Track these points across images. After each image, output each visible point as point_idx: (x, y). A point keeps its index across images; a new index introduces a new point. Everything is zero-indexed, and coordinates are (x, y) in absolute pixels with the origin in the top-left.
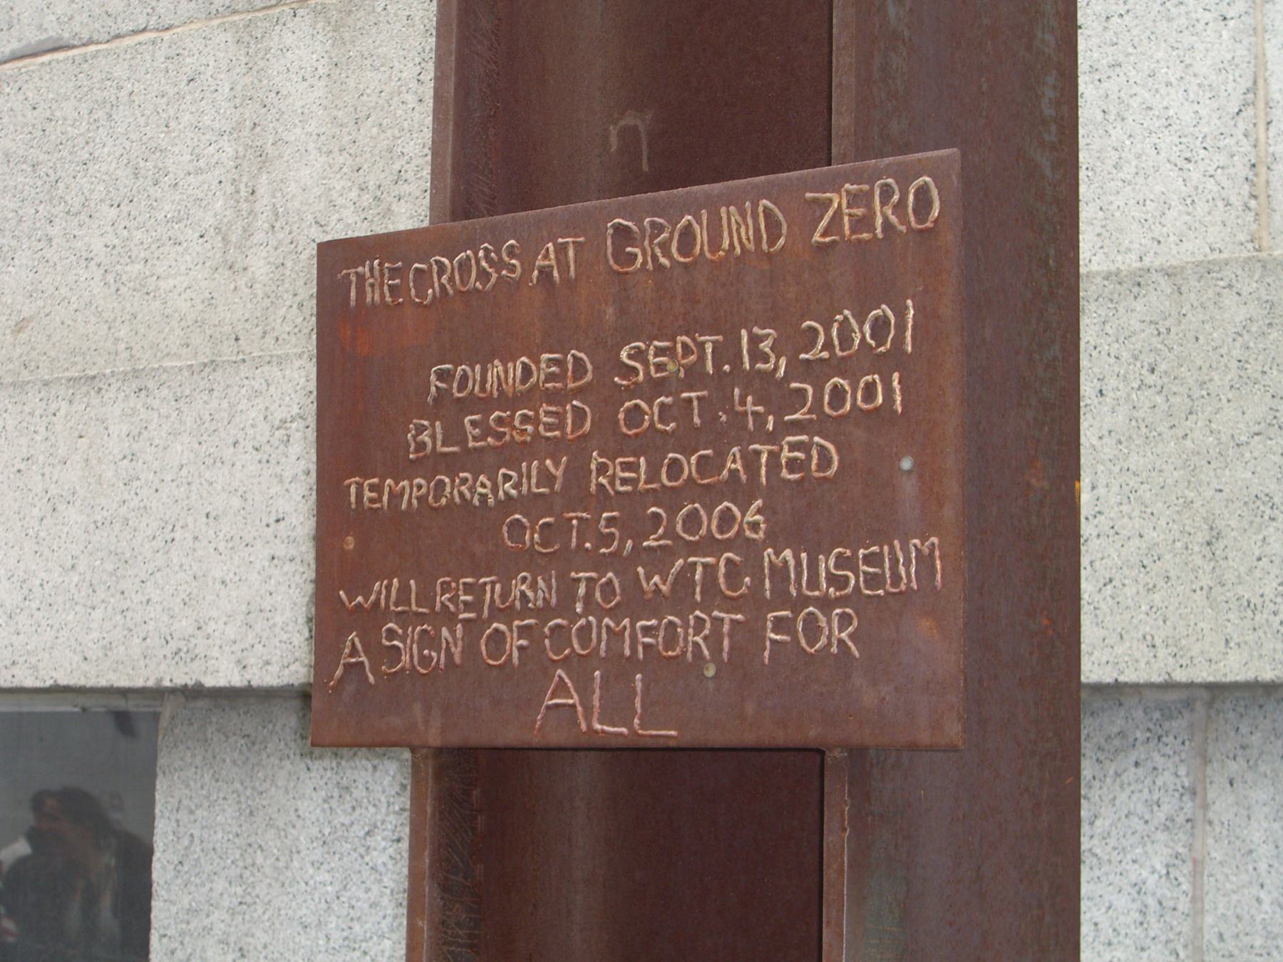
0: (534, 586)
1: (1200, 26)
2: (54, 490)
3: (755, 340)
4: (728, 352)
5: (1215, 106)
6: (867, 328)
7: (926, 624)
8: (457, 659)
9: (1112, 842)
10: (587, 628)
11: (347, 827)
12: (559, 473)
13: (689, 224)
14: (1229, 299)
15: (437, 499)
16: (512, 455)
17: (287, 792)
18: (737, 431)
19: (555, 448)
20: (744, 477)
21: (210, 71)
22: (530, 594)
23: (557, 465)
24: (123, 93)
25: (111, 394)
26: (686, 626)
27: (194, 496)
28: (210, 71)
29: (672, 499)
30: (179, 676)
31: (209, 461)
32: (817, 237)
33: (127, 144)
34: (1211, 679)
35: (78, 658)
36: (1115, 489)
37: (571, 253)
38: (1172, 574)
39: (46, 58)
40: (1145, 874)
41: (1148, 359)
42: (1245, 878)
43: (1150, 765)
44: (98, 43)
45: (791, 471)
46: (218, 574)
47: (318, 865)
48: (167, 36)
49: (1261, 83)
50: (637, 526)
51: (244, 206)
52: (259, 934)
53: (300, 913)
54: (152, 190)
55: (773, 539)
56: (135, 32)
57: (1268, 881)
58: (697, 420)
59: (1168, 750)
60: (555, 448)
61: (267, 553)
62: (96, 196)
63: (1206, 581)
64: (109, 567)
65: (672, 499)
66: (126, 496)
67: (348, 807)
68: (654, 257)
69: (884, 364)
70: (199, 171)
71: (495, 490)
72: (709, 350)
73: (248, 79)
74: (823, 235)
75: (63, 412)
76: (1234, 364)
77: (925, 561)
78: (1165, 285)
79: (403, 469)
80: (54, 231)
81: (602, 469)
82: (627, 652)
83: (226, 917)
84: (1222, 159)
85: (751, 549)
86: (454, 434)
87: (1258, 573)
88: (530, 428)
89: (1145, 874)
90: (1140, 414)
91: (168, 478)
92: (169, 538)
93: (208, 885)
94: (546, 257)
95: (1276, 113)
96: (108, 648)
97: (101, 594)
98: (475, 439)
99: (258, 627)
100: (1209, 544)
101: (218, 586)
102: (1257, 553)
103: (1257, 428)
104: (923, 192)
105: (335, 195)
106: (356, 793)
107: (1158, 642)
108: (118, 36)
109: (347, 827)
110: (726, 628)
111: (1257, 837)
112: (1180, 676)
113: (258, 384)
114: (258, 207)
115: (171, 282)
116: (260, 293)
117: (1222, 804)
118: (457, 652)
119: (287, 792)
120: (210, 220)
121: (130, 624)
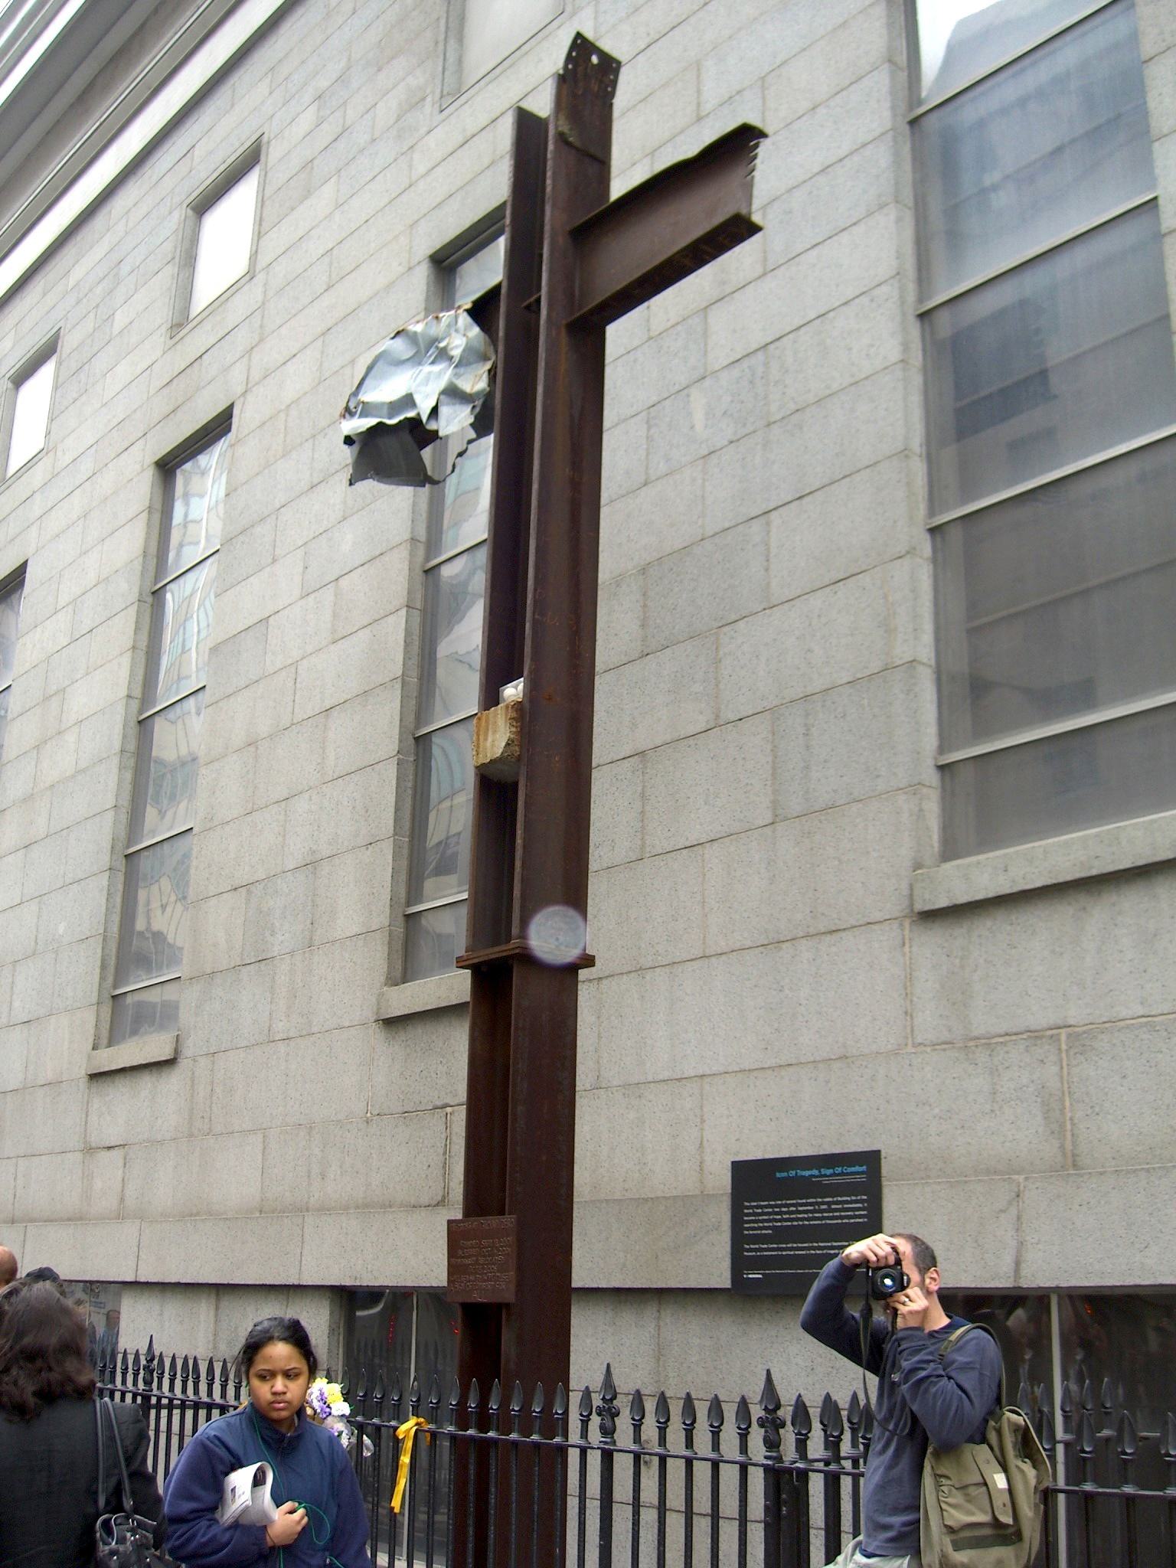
16: (469, 1256)
50: (483, 1269)
55: (498, 1271)
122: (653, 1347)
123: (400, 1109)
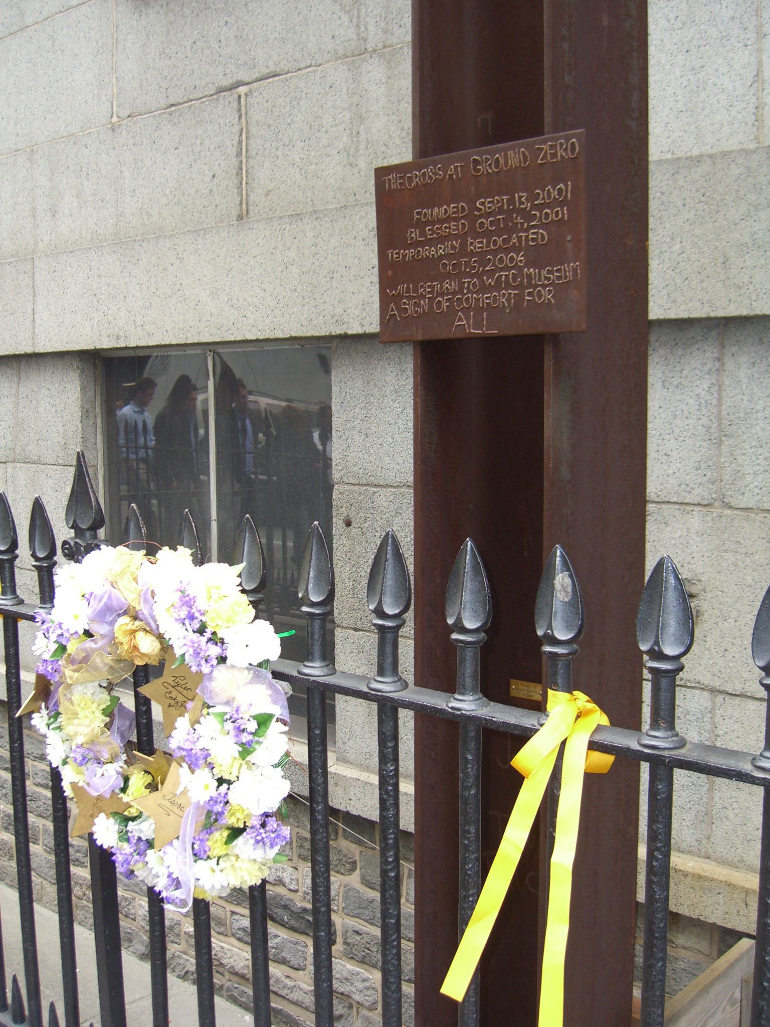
0: (450, 285)
1: (736, 49)
2: (286, 260)
3: (520, 197)
4: (511, 201)
5: (742, 83)
6: (556, 193)
7: (575, 292)
8: (426, 311)
9: (688, 379)
10: (468, 298)
11: (404, 386)
12: (457, 246)
13: (498, 158)
14: (733, 166)
15: (418, 256)
16: (442, 239)
17: (381, 373)
18: (514, 229)
19: (456, 237)
20: (517, 245)
21: (338, 83)
22: (449, 287)
23: (457, 243)
24: (303, 94)
25: (306, 220)
26: (500, 296)
27: (340, 259)
28: (338, 83)
29: (494, 253)
30: (337, 330)
31: (345, 245)
32: (539, 162)
33: (306, 115)
34: (724, 315)
35: (299, 325)
36: (689, 243)
37: (459, 169)
38: (710, 275)
39: (271, 80)
40: (700, 391)
41: (702, 191)
42: (737, 391)
43: (703, 349)
44: (291, 73)
45: (533, 242)
46: (351, 290)
47: (394, 401)
48: (320, 68)
49: (760, 73)
50: (483, 263)
51: (355, 139)
52: (373, 428)
53: (388, 419)
54: (317, 134)
55: (528, 265)
56: (306, 67)
57: (746, 392)
58: (502, 226)
59: (709, 343)
60: (456, 237)
61: (369, 281)
62: (294, 138)
63: (722, 278)
64: (309, 289)
65: (494, 253)
66: (314, 261)
67: (404, 378)
68: (487, 170)
69: (562, 204)
70: (337, 125)
71: (437, 252)
72: (505, 200)
73: (353, 86)
74: (542, 160)
75: (288, 229)
76: (734, 192)
77: (575, 270)
78: (709, 161)
79: (407, 246)
80: (279, 153)
81: (472, 244)
82: (481, 305)
83: (360, 422)
84: (744, 105)
85: (520, 269)
86: (422, 233)
87: (741, 274)
88: (448, 230)
89: (700, 391)
90: (698, 213)
91: (330, 253)
92: (331, 276)
93: (353, 411)
94: (451, 170)
95: (766, 85)
96: (310, 321)
97: (307, 300)
98: (430, 235)
99: (367, 310)
100: (724, 263)
101: (351, 295)
102: (741, 266)
103: (742, 217)
104: (573, 143)
105: (391, 132)
106: (407, 373)
107: (704, 302)
108: (299, 70)
109: (404, 386)
110: (512, 296)
111: (742, 375)
112: (713, 315)
113: (363, 214)
114: (360, 139)
115: (327, 172)
116: (363, 175)
117: (729, 363)
118: (426, 308)
119: (381, 373)
120: (342, 146)
121: (318, 311)
122: (705, 420)
123: (163, 103)
